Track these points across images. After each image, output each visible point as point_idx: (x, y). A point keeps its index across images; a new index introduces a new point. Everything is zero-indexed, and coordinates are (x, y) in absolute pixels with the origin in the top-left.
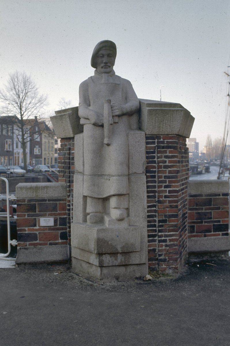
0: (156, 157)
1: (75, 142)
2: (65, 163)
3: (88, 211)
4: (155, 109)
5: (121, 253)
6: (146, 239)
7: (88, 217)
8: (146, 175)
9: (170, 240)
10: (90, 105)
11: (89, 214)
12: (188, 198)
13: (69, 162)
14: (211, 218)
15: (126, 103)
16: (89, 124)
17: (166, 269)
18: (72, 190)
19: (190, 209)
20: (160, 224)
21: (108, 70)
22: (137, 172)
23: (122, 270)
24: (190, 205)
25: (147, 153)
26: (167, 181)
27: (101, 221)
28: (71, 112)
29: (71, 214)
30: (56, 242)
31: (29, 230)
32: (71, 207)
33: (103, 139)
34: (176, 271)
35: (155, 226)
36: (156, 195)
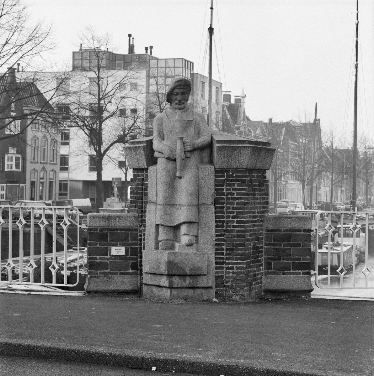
0: (225, 189)
1: (149, 174)
2: (137, 193)
3: (160, 239)
4: (223, 146)
5: (189, 275)
6: (214, 265)
7: (160, 243)
8: (215, 206)
9: (237, 268)
10: (164, 139)
11: (160, 241)
12: (264, 232)
13: (142, 193)
14: (290, 255)
15: (199, 137)
16: (163, 157)
17: (233, 296)
18: (145, 220)
19: (266, 245)
20: (228, 252)
21: (182, 106)
22: (206, 203)
23: (190, 292)
24: (267, 241)
25: (216, 185)
26: (235, 212)
27: (172, 247)
28: (146, 144)
29: (142, 244)
30: (126, 271)
31: (100, 259)
32: (143, 237)
33: (175, 172)
34: (243, 298)
35: (223, 254)
36: (224, 225)
